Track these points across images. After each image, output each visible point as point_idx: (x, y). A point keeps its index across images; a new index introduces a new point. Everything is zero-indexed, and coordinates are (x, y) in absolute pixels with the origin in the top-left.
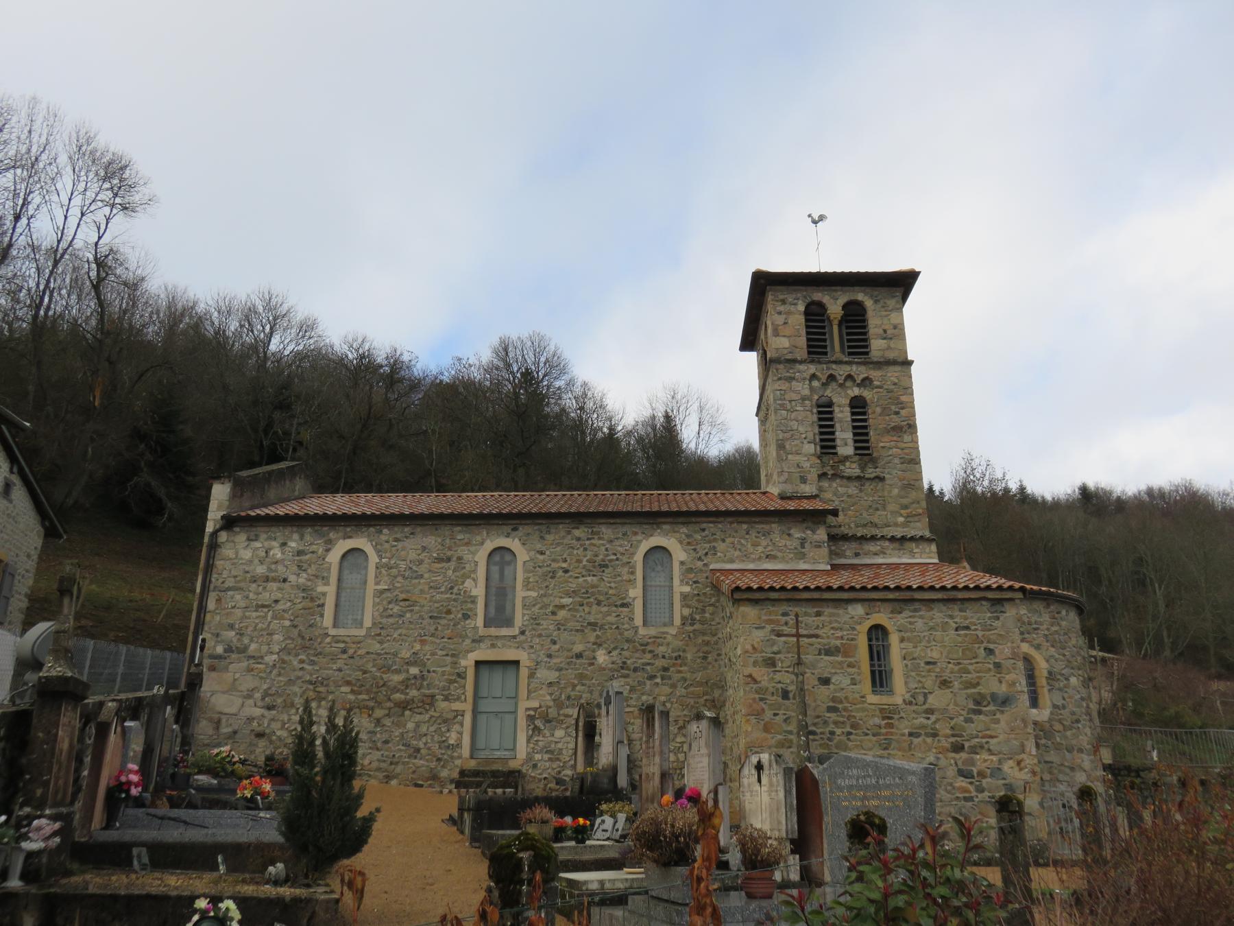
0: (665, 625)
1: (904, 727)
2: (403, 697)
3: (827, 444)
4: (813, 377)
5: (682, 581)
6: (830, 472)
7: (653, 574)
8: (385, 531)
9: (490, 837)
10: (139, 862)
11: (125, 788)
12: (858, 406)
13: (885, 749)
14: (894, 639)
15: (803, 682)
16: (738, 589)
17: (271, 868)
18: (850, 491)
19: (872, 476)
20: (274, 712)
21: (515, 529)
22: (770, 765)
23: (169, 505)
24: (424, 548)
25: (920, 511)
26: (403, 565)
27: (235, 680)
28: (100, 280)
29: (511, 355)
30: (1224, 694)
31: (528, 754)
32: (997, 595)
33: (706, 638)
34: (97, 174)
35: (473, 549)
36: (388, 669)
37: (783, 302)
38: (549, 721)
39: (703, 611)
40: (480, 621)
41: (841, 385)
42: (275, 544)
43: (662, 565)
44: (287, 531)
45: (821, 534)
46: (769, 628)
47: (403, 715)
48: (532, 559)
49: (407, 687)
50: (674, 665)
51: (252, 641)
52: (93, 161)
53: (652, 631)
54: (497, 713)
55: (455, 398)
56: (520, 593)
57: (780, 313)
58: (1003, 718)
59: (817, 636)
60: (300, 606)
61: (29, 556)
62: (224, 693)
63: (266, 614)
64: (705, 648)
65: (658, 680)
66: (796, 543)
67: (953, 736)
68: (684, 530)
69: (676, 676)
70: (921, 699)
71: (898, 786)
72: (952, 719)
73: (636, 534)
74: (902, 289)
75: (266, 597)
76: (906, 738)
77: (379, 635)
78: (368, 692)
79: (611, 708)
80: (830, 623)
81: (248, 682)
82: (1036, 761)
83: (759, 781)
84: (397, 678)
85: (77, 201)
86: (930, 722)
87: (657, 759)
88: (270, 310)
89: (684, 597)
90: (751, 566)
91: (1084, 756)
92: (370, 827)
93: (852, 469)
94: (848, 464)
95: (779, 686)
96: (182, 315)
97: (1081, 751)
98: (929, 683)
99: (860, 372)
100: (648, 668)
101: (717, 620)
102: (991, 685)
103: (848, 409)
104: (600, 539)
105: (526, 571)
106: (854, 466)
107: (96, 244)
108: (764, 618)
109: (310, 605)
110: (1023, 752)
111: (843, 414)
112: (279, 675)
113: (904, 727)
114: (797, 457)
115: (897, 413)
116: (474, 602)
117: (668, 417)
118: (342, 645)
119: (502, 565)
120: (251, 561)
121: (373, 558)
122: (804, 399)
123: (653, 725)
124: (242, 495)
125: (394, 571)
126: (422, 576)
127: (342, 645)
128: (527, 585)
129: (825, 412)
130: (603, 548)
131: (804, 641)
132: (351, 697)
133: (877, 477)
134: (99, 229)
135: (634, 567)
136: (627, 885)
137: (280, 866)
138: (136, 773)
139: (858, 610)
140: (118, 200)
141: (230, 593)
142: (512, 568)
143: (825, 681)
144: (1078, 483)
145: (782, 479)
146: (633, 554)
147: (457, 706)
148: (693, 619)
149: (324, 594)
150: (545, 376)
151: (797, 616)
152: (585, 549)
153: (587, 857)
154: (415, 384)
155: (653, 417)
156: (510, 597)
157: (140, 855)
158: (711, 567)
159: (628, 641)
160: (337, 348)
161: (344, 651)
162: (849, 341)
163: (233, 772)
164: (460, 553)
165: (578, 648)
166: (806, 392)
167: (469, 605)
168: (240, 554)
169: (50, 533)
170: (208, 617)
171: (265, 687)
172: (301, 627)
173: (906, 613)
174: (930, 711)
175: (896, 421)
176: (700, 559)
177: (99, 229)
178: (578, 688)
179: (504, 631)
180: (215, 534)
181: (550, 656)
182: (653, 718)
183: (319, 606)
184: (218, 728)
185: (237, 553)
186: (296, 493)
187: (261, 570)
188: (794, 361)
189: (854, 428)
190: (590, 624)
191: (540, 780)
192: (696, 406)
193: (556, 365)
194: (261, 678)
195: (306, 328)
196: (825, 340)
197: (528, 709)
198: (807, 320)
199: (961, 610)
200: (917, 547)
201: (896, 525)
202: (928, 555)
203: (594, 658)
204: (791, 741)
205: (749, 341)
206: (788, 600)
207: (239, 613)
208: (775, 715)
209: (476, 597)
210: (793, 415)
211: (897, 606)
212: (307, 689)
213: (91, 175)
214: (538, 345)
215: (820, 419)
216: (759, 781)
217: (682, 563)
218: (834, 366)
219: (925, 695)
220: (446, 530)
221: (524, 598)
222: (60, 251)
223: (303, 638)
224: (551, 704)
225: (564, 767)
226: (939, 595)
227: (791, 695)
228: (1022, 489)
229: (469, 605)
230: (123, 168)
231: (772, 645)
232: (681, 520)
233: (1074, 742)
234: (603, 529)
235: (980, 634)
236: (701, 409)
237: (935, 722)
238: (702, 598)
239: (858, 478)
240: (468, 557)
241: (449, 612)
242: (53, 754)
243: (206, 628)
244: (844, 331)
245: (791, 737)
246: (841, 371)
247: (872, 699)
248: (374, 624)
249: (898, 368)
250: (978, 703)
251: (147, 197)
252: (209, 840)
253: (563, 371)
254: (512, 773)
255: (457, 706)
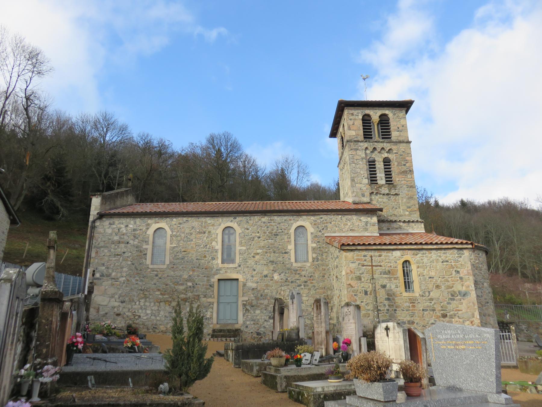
0: (305, 262)
1: (420, 307)
2: (185, 296)
3: (373, 179)
4: (367, 148)
5: (312, 242)
6: (375, 192)
7: (299, 239)
8: (174, 220)
9: (246, 363)
10: (91, 383)
11: (76, 345)
12: (387, 162)
13: (412, 317)
14: (413, 267)
15: (375, 287)
16: (343, 245)
17: (161, 386)
18: (384, 200)
19: (394, 193)
20: (124, 304)
21: (235, 218)
22: (394, 328)
23: (62, 210)
24: (193, 228)
25: (416, 209)
26: (183, 235)
27: (106, 289)
28: (28, 106)
29: (215, 142)
30: (529, 289)
31: (244, 321)
32: (460, 246)
33: (324, 267)
34: (25, 57)
35: (215, 228)
36: (177, 283)
37: (352, 114)
38: (253, 306)
39: (322, 255)
40: (220, 261)
41: (379, 152)
42: (122, 226)
43: (303, 234)
44: (128, 220)
45: (375, 219)
46: (358, 262)
47: (185, 304)
48: (243, 232)
49: (186, 291)
50: (310, 280)
51: (113, 271)
52: (23, 51)
53: (299, 265)
54: (228, 303)
55: (187, 162)
56: (238, 248)
57: (351, 120)
58: (464, 302)
59: (381, 266)
60: (135, 255)
61: (3, 233)
62: (100, 295)
63: (119, 259)
64: (324, 272)
65: (303, 287)
66: (363, 224)
67: (442, 310)
68: (312, 218)
69: (310, 285)
70: (427, 294)
71: (477, 339)
72: (441, 303)
73: (290, 220)
74: (406, 109)
75: (119, 251)
76: (421, 312)
77: (173, 267)
78: (168, 294)
79: (295, 301)
80: (386, 259)
81: (112, 291)
82: (479, 321)
83: (388, 335)
84: (182, 288)
85: (16, 69)
86: (431, 304)
87: (323, 325)
88: (106, 121)
89: (314, 249)
90: (343, 235)
91: (491, 319)
92: (211, 364)
93: (385, 190)
94: (383, 188)
95: (363, 289)
96: (64, 125)
97: (489, 315)
98: (431, 286)
99: (387, 146)
100: (298, 281)
101: (329, 259)
102: (458, 287)
103: (383, 163)
104: (274, 222)
105: (240, 237)
106: (386, 189)
107: (26, 89)
108: (355, 258)
109: (140, 254)
110: (473, 317)
111: (380, 166)
112: (126, 287)
113: (420, 307)
114: (360, 185)
115: (405, 165)
116: (216, 252)
117: (282, 170)
118: (156, 273)
119: (230, 234)
120: (111, 234)
121: (169, 232)
122: (362, 159)
123: (320, 309)
124: (106, 204)
125: (179, 238)
126: (192, 240)
127: (156, 273)
128: (241, 244)
129: (372, 164)
130: (276, 227)
131: (374, 268)
132: (161, 296)
133: (396, 194)
134: (27, 82)
135: (290, 235)
136: (335, 389)
137: (166, 384)
138: (80, 337)
139: (397, 253)
140: (35, 69)
141: (102, 249)
142: (234, 236)
143: (384, 287)
144: (460, 199)
145: (354, 195)
146: (290, 229)
147: (210, 300)
148: (318, 259)
149: (147, 249)
150: (230, 151)
151: (371, 257)
152: (268, 227)
153: (304, 373)
154: (172, 155)
155: (278, 170)
156: (233, 249)
157: (91, 379)
158: (325, 235)
159: (288, 269)
160: (135, 139)
161: (157, 275)
162: (382, 132)
163: (115, 333)
164: (209, 229)
165: (265, 273)
166: (364, 156)
167: (215, 254)
168: (106, 230)
169: (13, 222)
170: (92, 260)
171: (120, 292)
172: (136, 265)
173: (420, 255)
174: (432, 299)
175: (404, 168)
176: (320, 231)
177: (27, 82)
178: (266, 291)
179: (231, 265)
180: (94, 222)
181: (252, 276)
182: (320, 305)
183: (144, 254)
184: (98, 312)
185: (105, 230)
186: (129, 203)
187: (116, 238)
188: (358, 141)
189: (385, 172)
190: (270, 261)
191: (249, 333)
192: (296, 165)
193: (235, 147)
194: (118, 288)
195: (123, 129)
196: (371, 132)
197: (243, 301)
198: (363, 123)
199: (444, 253)
200: (415, 225)
201: (405, 215)
202: (420, 229)
203: (273, 277)
204: (369, 314)
205: (333, 134)
206: (366, 250)
207: (106, 258)
208: (362, 302)
209: (218, 250)
210: (358, 166)
211: (415, 252)
212: (140, 293)
213: (23, 57)
214: (227, 138)
215: (370, 168)
216: (388, 335)
217: (312, 233)
218: (376, 144)
219: (429, 292)
220: (203, 219)
221: (240, 250)
222: (9, 92)
223: (137, 269)
224: (254, 298)
225: (260, 327)
226: (435, 247)
227: (369, 293)
228: (436, 203)
229: (215, 254)
230: (38, 54)
231: (359, 271)
232: (311, 213)
233: (486, 312)
234: (276, 218)
235: (453, 264)
236: (299, 167)
237: (433, 305)
238: (322, 249)
239: (388, 194)
240: (213, 231)
241: (205, 257)
242: (50, 330)
243: (91, 265)
244: (380, 128)
245: (369, 312)
246: (379, 146)
247: (405, 294)
248: (170, 263)
249: (405, 144)
250: (452, 295)
251: (49, 68)
252: (119, 369)
253: (239, 149)
254: (237, 330)
255: (210, 300)
